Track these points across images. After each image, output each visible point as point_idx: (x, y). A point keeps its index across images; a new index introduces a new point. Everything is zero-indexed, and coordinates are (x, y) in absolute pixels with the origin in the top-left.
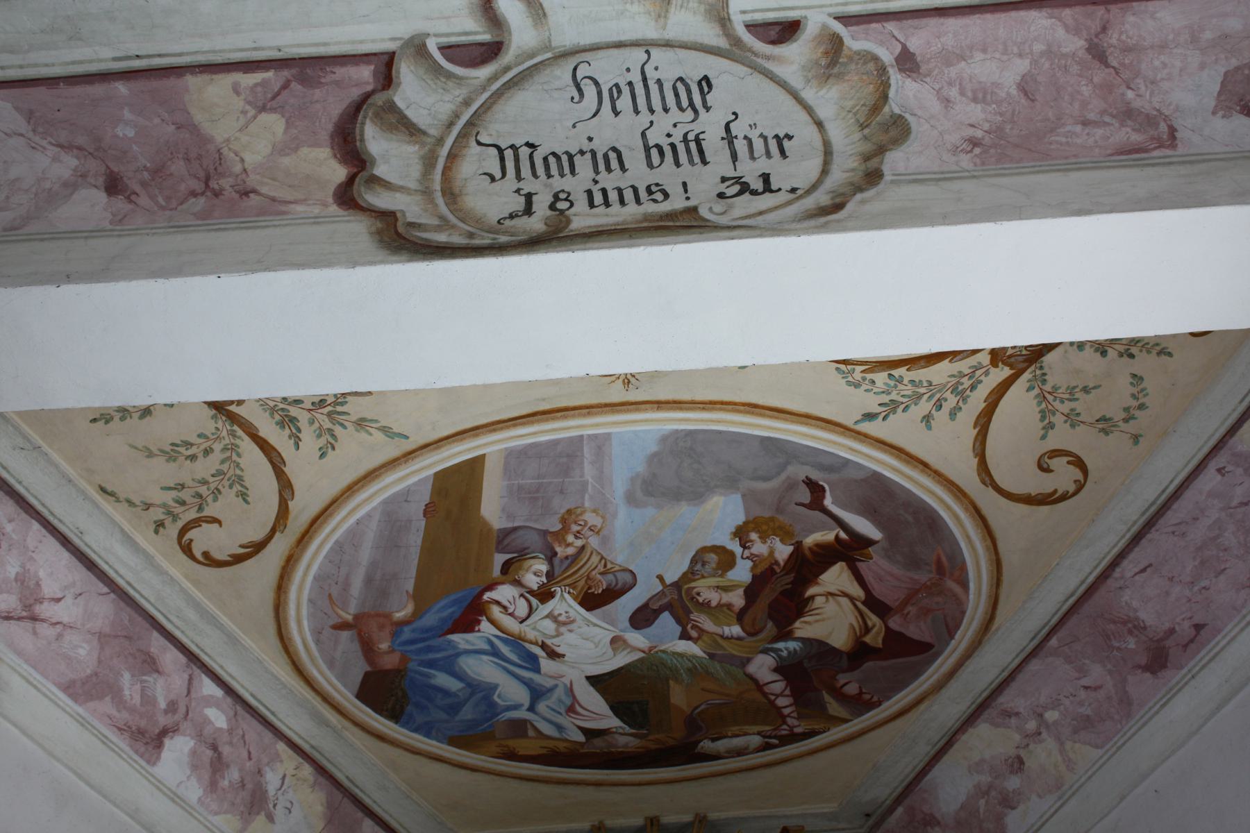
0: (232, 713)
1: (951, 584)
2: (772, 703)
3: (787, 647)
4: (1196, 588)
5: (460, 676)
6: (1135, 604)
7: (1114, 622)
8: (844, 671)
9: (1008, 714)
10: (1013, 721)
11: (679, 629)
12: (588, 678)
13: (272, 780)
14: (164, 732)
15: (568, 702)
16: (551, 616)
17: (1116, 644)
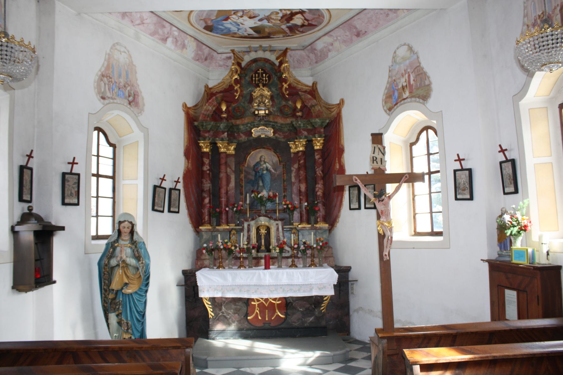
1: (321, 18)
2: (285, 32)
3: (288, 24)
5: (224, 26)
6: (356, 24)
9: (331, 36)
10: (332, 37)
13: (186, 42)
14: (167, 38)
16: (243, 19)
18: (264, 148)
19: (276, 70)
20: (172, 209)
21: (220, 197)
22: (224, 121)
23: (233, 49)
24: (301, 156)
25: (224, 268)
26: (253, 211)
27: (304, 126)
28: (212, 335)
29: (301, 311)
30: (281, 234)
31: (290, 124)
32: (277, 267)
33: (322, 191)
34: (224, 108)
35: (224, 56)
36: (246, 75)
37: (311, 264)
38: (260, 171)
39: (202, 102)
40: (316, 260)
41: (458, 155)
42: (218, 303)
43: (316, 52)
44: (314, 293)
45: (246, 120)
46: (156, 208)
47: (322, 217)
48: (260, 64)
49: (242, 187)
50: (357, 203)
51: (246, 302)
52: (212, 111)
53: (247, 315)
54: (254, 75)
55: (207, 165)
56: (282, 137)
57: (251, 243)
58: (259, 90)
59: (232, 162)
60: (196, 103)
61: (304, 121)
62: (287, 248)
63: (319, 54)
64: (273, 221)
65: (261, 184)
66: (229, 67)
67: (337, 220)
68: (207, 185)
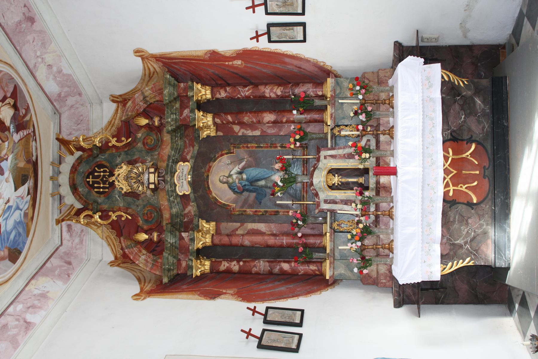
0: (18, 303)
2: (25, 136)
3: (12, 129)
4: (13, 3)
6: (13, 21)
7: (16, 29)
8: (19, 113)
9: (35, 66)
10: (37, 65)
11: (5, 161)
12: (15, 191)
13: (36, 292)
14: (26, 322)
15: (20, 198)
17: (23, 30)
18: (208, 176)
19: (89, 156)
20: (298, 321)
21: (281, 246)
22: (164, 236)
23: (54, 221)
24: (220, 119)
25: (392, 241)
26: (303, 196)
27: (176, 114)
28: (500, 264)
29: (465, 118)
30: (341, 152)
31: (172, 136)
32: (392, 158)
33: (276, 87)
34: (143, 237)
35: (65, 235)
36: (96, 202)
37: (389, 104)
38: (243, 184)
39: (133, 271)
40: (383, 96)
41: (247, 8)
42: (450, 250)
43: (63, 95)
44: (437, 95)
45: (164, 203)
46: (294, 346)
47: (315, 88)
48: (79, 180)
49: (266, 212)
50: (295, 28)
51: (449, 205)
52: (148, 254)
53: (470, 204)
54: (96, 190)
55: (230, 265)
56: (191, 148)
57: (353, 199)
58: (119, 181)
59: (228, 226)
60: (136, 280)
61: (168, 113)
62: (363, 143)
63: (66, 89)
64: (320, 163)
65: (262, 183)
66: (84, 228)
67: (322, 64)
68: (262, 265)
